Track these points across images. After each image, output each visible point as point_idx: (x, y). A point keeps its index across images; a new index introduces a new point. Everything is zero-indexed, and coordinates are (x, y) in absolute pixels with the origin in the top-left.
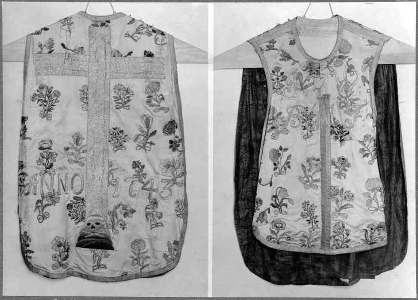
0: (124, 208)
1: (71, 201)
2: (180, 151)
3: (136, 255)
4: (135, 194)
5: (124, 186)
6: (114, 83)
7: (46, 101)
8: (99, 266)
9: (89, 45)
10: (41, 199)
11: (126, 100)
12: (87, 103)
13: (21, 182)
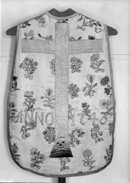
0: (78, 131)
1: (46, 129)
2: (110, 94)
3: (86, 160)
4: (84, 123)
5: (77, 119)
6: (70, 57)
7: (29, 68)
8: (64, 168)
9: (55, 34)
10: (25, 125)
11: (78, 67)
12: (55, 70)
13: (13, 115)
